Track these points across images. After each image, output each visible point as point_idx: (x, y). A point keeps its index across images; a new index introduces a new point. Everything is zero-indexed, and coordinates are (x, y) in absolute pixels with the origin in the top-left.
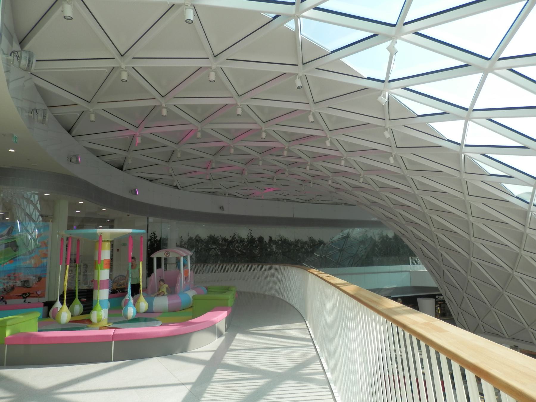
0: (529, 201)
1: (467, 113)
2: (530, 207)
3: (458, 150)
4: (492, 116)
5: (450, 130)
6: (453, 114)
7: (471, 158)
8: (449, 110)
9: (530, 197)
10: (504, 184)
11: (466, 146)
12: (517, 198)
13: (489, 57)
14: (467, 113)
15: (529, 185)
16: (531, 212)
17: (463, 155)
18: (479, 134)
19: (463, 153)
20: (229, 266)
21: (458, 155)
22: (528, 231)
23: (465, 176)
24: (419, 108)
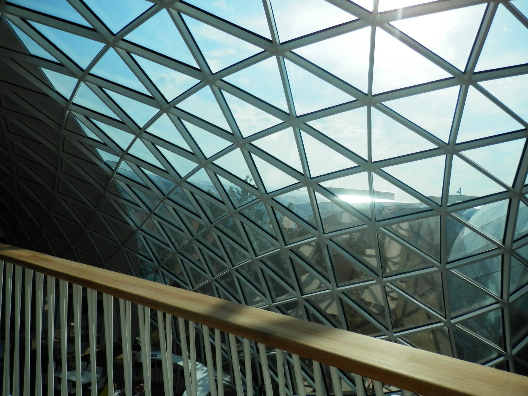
0: (114, 169)
1: (83, 75)
2: (113, 174)
3: (111, 174)
4: (102, 86)
5: (62, 84)
6: (68, 68)
7: (74, 116)
8: (65, 65)
9: (115, 165)
10: (98, 150)
11: (117, 173)
12: (105, 164)
13: (115, 33)
14: (83, 75)
15: (117, 155)
16: (114, 178)
17: (68, 112)
18: (87, 98)
19: (69, 110)
20: (286, 337)
21: (64, 110)
22: (107, 194)
23: (64, 132)
24: (35, 49)
